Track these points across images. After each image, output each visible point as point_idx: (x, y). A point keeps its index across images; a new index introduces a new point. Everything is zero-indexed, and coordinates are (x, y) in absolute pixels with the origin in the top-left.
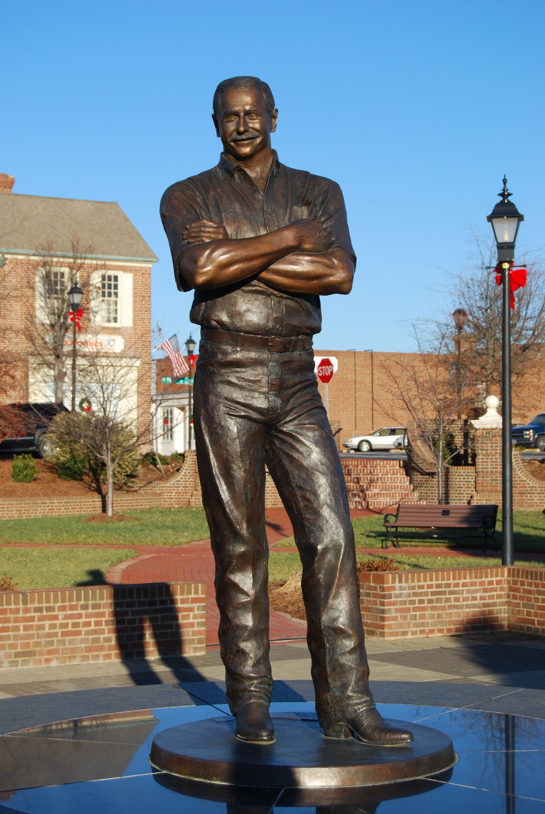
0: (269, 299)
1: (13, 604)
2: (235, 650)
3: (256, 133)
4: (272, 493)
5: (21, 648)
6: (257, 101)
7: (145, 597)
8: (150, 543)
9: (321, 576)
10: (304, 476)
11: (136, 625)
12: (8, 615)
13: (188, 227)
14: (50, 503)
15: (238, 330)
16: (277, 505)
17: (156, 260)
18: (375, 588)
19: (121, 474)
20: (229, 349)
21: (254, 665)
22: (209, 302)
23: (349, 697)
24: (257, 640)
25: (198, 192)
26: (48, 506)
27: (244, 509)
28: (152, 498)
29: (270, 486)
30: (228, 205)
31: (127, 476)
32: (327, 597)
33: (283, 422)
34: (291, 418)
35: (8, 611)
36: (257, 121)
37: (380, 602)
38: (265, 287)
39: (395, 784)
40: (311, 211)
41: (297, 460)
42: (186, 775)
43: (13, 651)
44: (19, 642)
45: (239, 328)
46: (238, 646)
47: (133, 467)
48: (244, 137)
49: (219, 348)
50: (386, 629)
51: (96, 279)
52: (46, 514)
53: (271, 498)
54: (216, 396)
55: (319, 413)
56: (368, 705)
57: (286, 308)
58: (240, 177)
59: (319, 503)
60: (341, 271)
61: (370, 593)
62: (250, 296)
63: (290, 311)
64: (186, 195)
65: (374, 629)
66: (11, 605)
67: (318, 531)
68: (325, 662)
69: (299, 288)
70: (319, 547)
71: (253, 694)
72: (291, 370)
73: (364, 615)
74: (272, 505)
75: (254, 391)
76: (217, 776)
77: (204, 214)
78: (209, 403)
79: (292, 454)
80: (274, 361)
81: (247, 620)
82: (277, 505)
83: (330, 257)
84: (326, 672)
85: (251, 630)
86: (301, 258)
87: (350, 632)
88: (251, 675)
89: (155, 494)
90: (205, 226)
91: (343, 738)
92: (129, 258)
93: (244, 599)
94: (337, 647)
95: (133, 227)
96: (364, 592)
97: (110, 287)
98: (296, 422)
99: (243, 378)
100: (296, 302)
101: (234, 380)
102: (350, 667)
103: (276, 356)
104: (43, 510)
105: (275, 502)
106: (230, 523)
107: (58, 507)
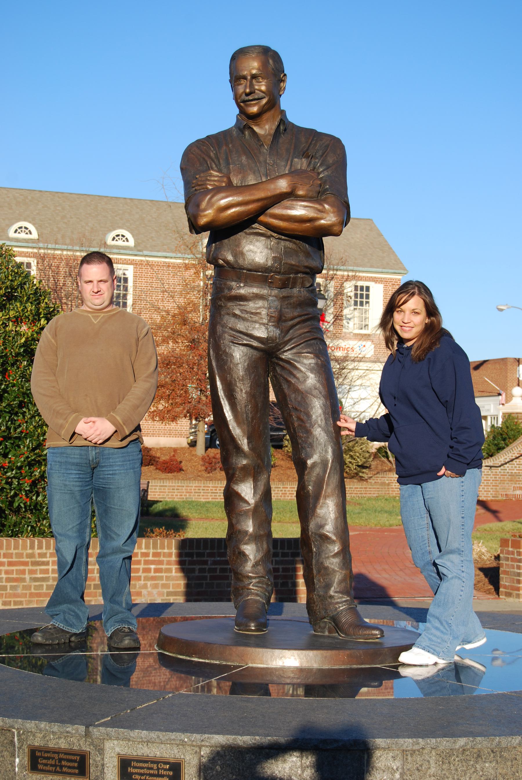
0: (269, 240)
1: (166, 548)
2: (237, 553)
3: (262, 94)
4: (493, 486)
5: (173, 588)
6: (264, 65)
7: (288, 549)
8: (363, 524)
9: (310, 487)
10: (299, 399)
11: (279, 574)
12: (162, 558)
13: (197, 177)
14: (283, 488)
15: (242, 268)
16: (498, 497)
17: (405, 272)
18: (513, 553)
19: (353, 464)
20: (234, 284)
21: (254, 566)
22: (217, 243)
23: (331, 597)
24: (256, 544)
25: (213, 147)
26: (281, 491)
27: (245, 427)
28: (380, 487)
29: (491, 479)
30: (236, 158)
31: (358, 466)
32: (315, 507)
33: (282, 350)
34: (289, 347)
35: (162, 554)
36: (263, 83)
37: (517, 565)
38: (265, 229)
39: (351, 669)
40: (310, 163)
41: (294, 385)
42: (174, 653)
43: (165, 591)
44: (171, 583)
45: (242, 266)
46: (239, 548)
47: (365, 458)
48: (250, 98)
49: (225, 284)
50: (521, 591)
51: (349, 288)
52: (279, 498)
53: (491, 490)
54: (223, 326)
55: (317, 344)
56: (347, 604)
57: (285, 248)
58: (249, 134)
59: (311, 423)
60: (332, 215)
61: (508, 558)
62: (252, 237)
63: (288, 252)
64: (201, 150)
65: (511, 591)
66: (164, 549)
67: (308, 447)
68: (312, 565)
69: (293, 230)
70: (309, 462)
71: (251, 592)
72: (290, 304)
73: (503, 578)
74: (493, 497)
75: (255, 322)
76: (195, 654)
77: (214, 166)
78: (217, 332)
79: (289, 379)
80: (273, 296)
81: (248, 526)
82: (498, 497)
83: (322, 202)
84: (313, 574)
85: (251, 535)
86: (295, 203)
87: (334, 538)
88: (250, 574)
89: (383, 484)
90: (211, 175)
91: (327, 633)
92: (380, 270)
93: (246, 507)
94: (322, 552)
95: (386, 241)
96: (504, 557)
97: (362, 296)
98: (294, 351)
99: (246, 311)
100: (295, 243)
101: (237, 312)
102: (333, 570)
103: (275, 292)
104: (277, 493)
105: (496, 494)
106: (232, 439)
107: (291, 492)
